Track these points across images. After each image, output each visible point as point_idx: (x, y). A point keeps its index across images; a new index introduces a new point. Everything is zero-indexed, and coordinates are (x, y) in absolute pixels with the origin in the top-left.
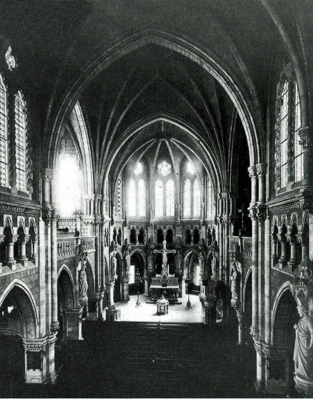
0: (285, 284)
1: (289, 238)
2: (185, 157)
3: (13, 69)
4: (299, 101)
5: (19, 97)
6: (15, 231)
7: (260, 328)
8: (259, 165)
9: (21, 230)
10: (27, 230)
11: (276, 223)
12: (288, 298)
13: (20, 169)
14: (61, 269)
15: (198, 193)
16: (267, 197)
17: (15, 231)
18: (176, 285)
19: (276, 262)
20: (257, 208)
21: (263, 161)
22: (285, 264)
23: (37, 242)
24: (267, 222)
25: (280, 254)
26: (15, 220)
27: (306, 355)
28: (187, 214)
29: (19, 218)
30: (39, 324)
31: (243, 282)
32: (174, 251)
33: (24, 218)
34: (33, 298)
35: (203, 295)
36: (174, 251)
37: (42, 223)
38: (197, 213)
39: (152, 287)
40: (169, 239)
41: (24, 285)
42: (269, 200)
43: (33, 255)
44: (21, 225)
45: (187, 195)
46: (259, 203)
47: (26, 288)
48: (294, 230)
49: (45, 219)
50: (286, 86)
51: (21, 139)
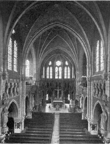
0: (98, 101)
1: (99, 87)
2: (65, 60)
3: (14, 33)
4: (103, 54)
5: (15, 42)
6: (13, 84)
7: (89, 115)
8: (90, 65)
9: (11, 84)
10: (16, 84)
11: (95, 83)
12: (98, 105)
13: (9, 62)
14: (95, 105)
15: (69, 71)
16: (92, 74)
17: (13, 84)
18: (61, 100)
19: (95, 94)
20: (89, 78)
21: (91, 64)
22: (97, 95)
23: (19, 87)
24: (92, 82)
25: (96, 92)
26: (13, 80)
27: (101, 41)
28: (65, 77)
29: (14, 80)
30: (19, 114)
31: (84, 100)
32: (61, 90)
33: (16, 80)
34: (17, 105)
35: (71, 104)
36: (61, 90)
37: (21, 82)
38: (69, 77)
39: (54, 101)
40: (60, 86)
41: (15, 101)
42: (93, 75)
43: (18, 92)
44: (15, 82)
45: (65, 71)
46: (90, 76)
47: (16, 102)
48: (101, 85)
49: (22, 80)
50: (98, 41)
51: (10, 52)
